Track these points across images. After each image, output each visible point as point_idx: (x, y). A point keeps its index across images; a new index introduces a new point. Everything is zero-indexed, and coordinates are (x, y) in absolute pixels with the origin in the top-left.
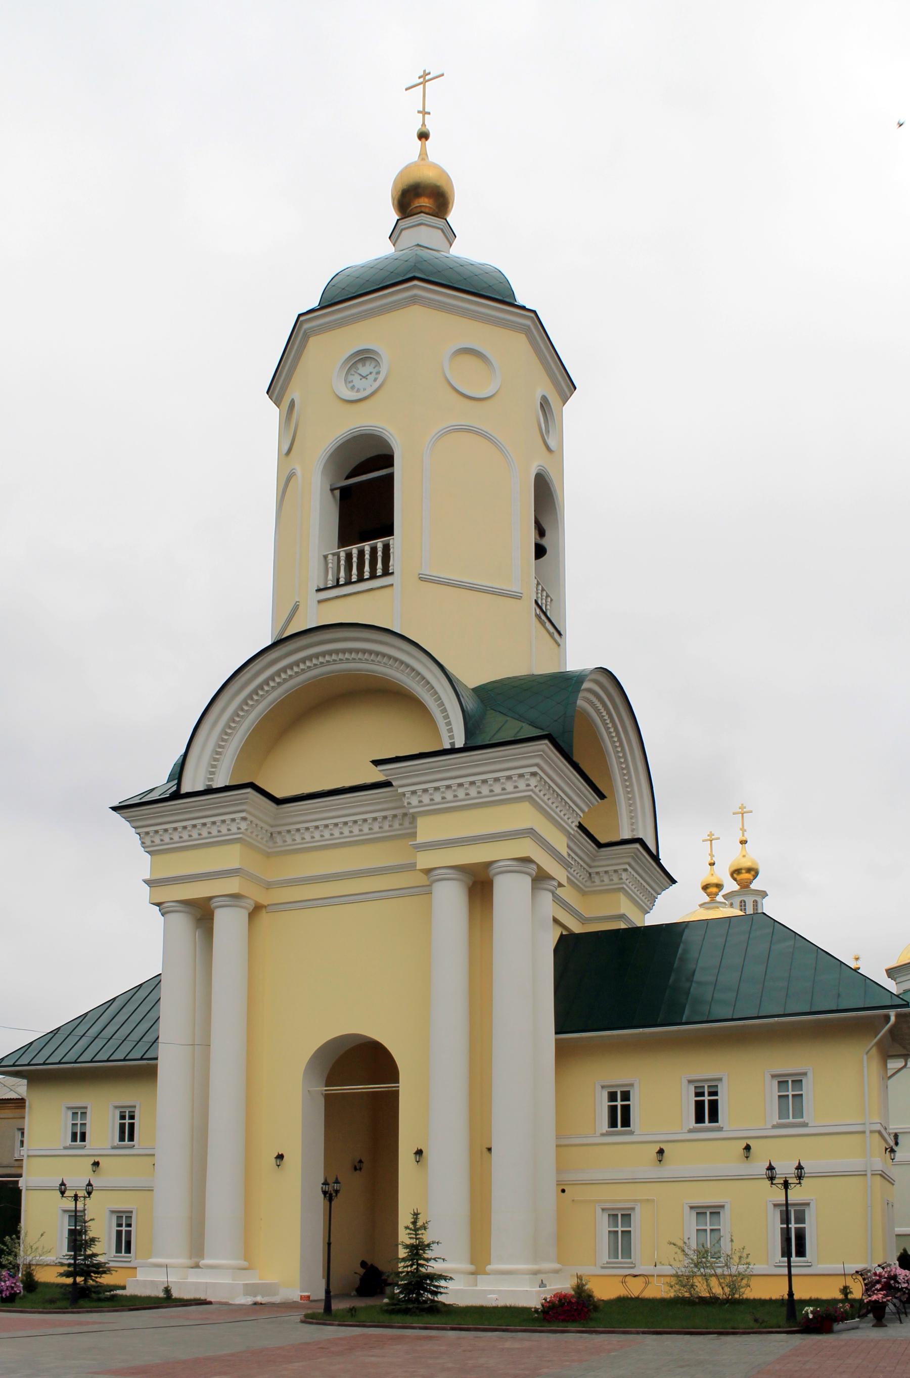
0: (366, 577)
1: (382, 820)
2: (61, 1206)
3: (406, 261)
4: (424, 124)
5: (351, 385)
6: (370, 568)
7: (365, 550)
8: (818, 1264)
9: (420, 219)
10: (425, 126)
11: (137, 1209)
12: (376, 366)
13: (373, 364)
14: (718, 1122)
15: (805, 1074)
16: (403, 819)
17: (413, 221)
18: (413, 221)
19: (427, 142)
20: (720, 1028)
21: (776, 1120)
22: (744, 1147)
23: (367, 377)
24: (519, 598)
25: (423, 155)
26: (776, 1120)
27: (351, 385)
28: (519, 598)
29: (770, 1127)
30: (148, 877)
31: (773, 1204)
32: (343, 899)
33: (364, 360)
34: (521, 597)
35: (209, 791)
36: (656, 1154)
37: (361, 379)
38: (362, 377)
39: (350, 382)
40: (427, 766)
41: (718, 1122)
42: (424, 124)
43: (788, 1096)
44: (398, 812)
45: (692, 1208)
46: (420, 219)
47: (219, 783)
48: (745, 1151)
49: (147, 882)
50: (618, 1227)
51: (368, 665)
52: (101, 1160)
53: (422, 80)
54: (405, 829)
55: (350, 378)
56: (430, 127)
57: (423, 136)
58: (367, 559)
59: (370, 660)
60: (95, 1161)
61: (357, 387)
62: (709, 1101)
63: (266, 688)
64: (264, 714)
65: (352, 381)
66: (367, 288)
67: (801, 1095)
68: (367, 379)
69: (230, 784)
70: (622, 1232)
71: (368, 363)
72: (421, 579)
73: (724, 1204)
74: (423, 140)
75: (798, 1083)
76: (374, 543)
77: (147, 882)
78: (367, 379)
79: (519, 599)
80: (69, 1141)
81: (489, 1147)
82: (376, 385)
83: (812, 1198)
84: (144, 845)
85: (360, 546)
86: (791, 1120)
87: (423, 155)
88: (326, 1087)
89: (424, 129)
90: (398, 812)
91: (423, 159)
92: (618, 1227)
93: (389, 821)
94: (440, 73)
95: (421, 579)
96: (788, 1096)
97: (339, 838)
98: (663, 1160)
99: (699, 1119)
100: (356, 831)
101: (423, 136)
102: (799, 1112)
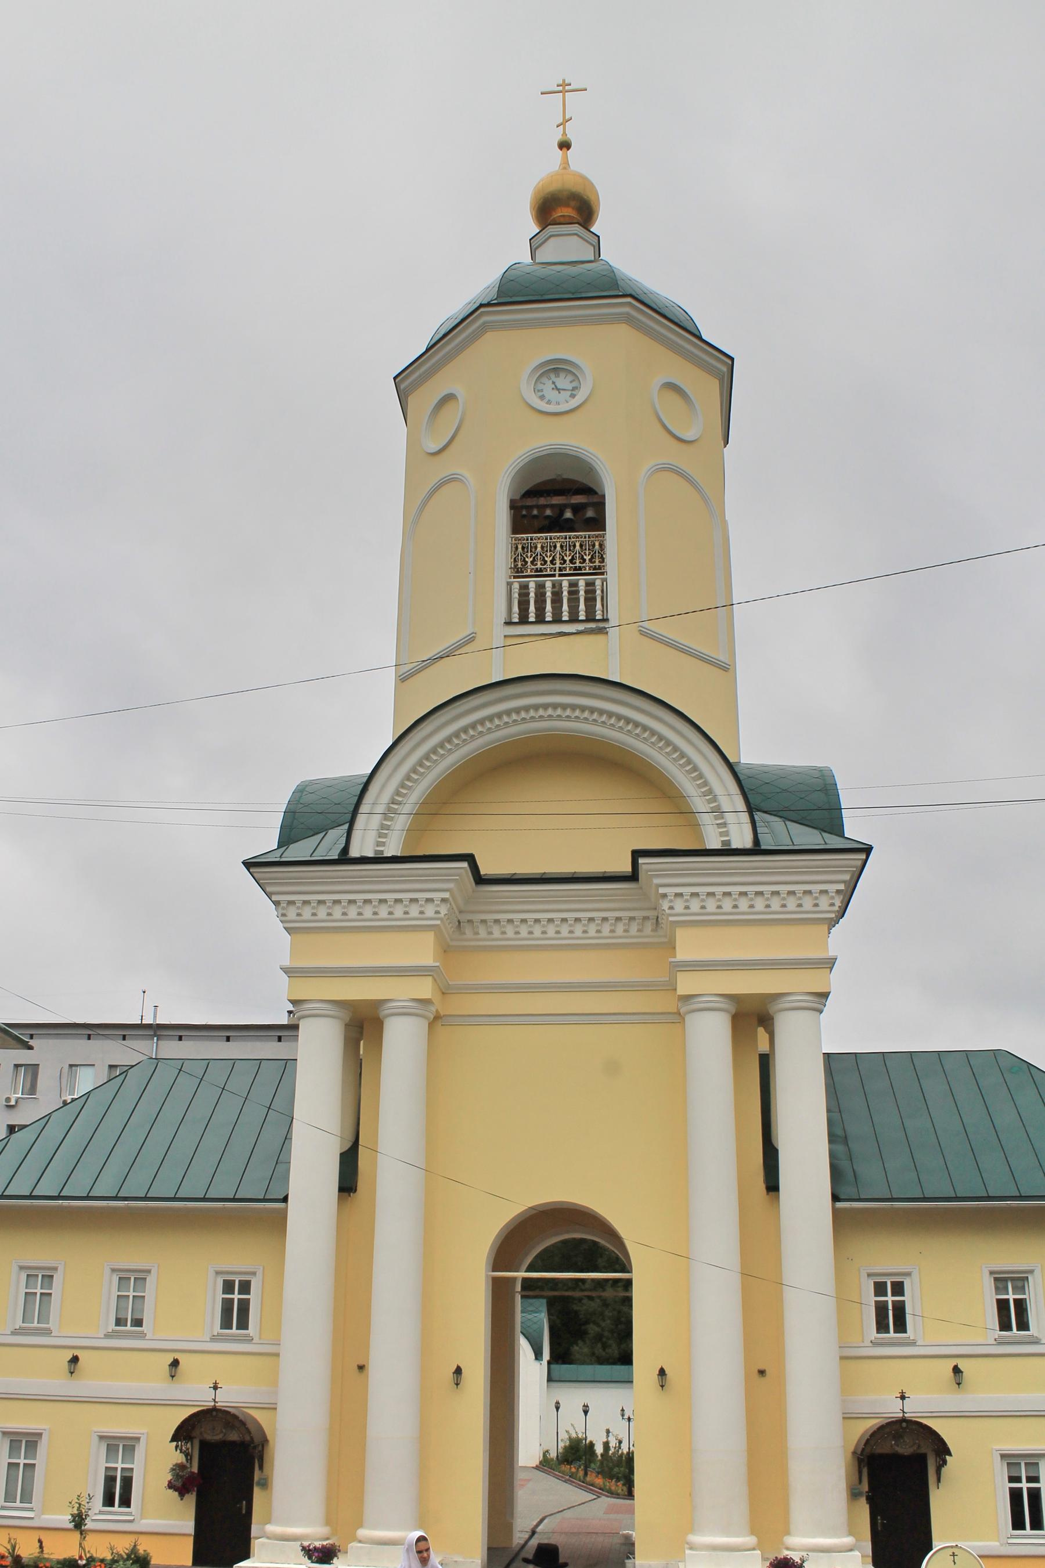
0: (548, 619)
1: (615, 921)
2: (96, 1429)
3: (559, 272)
4: (564, 134)
5: (540, 394)
6: (535, 608)
7: (530, 587)
8: (141, 1519)
9: (548, 231)
10: (566, 135)
11: (148, 1433)
12: (574, 380)
13: (570, 378)
14: (248, 1329)
15: (149, 1271)
16: (615, 925)
17: (582, 232)
18: (582, 232)
19: (568, 152)
20: (235, 1209)
21: (19, 1323)
22: (453, 1370)
23: (561, 392)
24: (727, 670)
25: (565, 164)
26: (19, 1323)
27: (540, 394)
28: (727, 670)
29: (9, 1333)
30: (287, 963)
31: (98, 1435)
32: (493, 1019)
33: (556, 371)
34: (729, 669)
35: (379, 860)
36: (168, 1366)
37: (553, 389)
38: (554, 387)
39: (538, 391)
40: (820, 863)
41: (248, 1329)
42: (564, 134)
43: (36, 1293)
44: (651, 914)
45: (101, 1438)
46: (548, 231)
47: (391, 850)
48: (455, 1375)
49: (287, 971)
50: (19, 1464)
51: (579, 724)
52: (182, 1358)
53: (561, 88)
54: (632, 937)
55: (540, 386)
56: (571, 137)
57: (565, 145)
58: (549, 596)
59: (582, 718)
60: (73, 1355)
61: (548, 397)
62: (239, 1299)
63: (463, 736)
64: (661, 770)
65: (542, 390)
66: (514, 296)
67: (50, 1294)
68: (559, 393)
69: (402, 855)
70: (25, 1464)
71: (562, 375)
72: (642, 632)
73: (140, 1435)
74: (565, 149)
75: (141, 1281)
76: (543, 580)
77: (287, 971)
78: (559, 393)
79: (726, 671)
80: (112, 1326)
81: (361, 1363)
82: (573, 403)
83: (142, 1431)
84: (283, 918)
85: (524, 581)
86: (36, 1324)
87: (565, 164)
88: (493, 1271)
89: (565, 139)
90: (651, 914)
91: (565, 168)
92: (19, 1464)
93: (611, 925)
94: (583, 87)
95: (642, 632)
96: (36, 1293)
97: (620, 937)
98: (177, 1375)
99: (226, 1324)
100: (537, 933)
101: (565, 145)
102: (43, 1317)
